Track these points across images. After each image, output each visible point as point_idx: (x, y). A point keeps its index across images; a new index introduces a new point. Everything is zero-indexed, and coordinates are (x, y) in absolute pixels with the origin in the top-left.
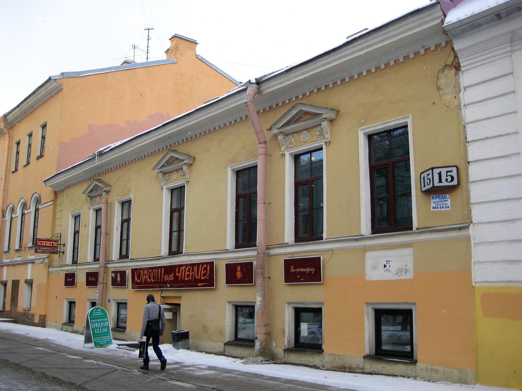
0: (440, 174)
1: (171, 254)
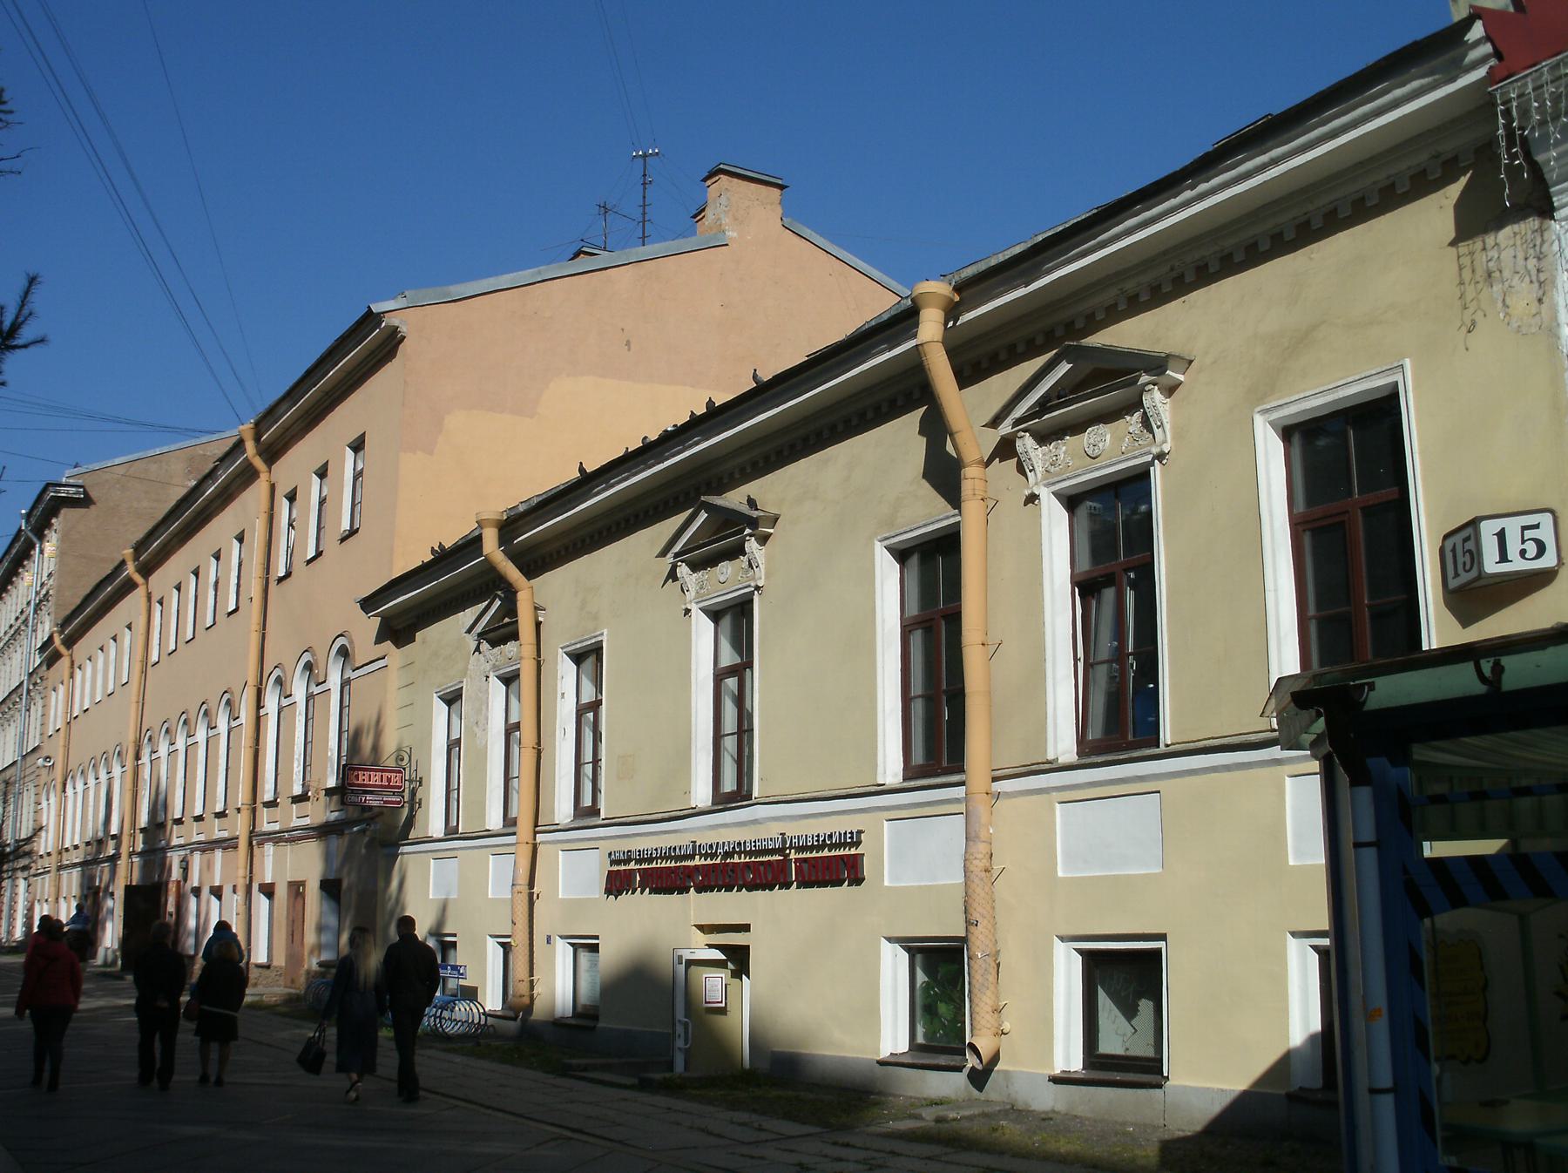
0: (1501, 536)
1: (723, 801)
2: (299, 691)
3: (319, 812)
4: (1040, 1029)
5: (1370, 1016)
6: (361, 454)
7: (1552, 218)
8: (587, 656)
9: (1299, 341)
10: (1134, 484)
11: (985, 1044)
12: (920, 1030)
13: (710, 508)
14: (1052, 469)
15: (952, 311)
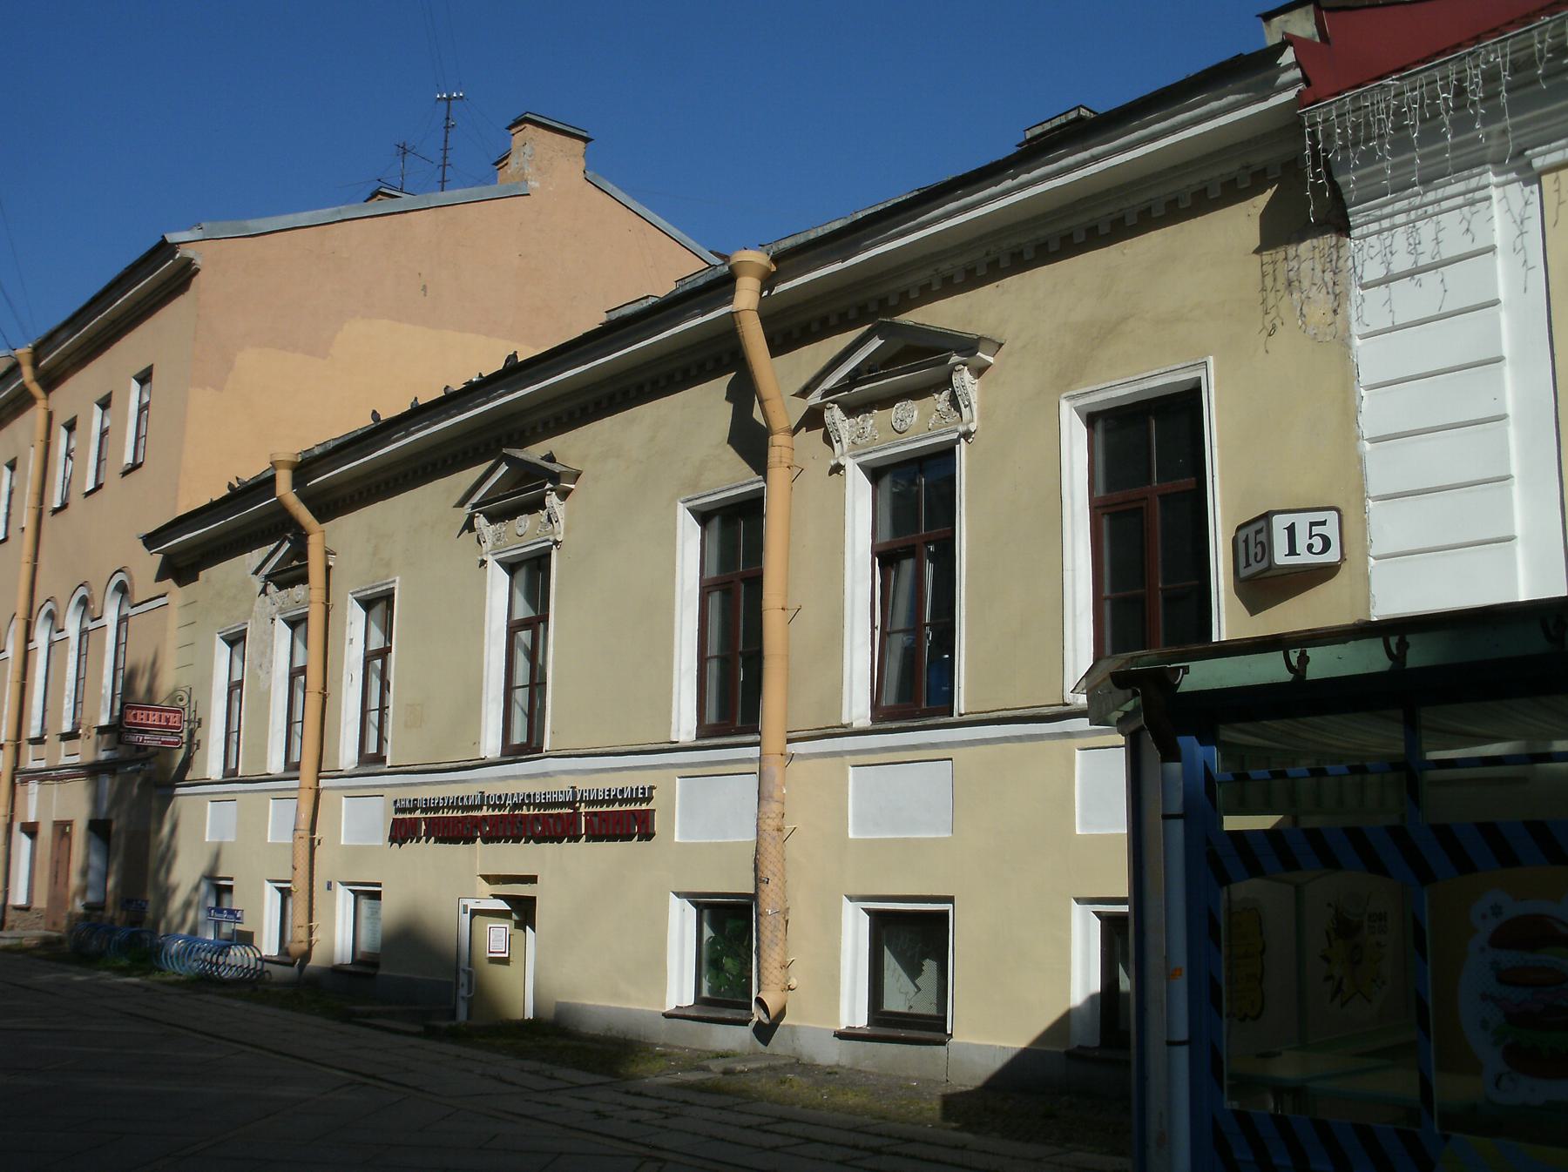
0: (1291, 530)
1: (513, 753)
2: (72, 627)
3: (87, 751)
4: (826, 984)
5: (1171, 975)
6: (147, 386)
7: (1348, 236)
8: (378, 603)
9: (1100, 335)
10: (943, 457)
11: (772, 999)
12: (705, 985)
13: (511, 461)
14: (859, 441)
15: (768, 281)
